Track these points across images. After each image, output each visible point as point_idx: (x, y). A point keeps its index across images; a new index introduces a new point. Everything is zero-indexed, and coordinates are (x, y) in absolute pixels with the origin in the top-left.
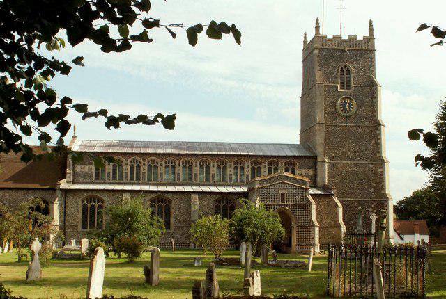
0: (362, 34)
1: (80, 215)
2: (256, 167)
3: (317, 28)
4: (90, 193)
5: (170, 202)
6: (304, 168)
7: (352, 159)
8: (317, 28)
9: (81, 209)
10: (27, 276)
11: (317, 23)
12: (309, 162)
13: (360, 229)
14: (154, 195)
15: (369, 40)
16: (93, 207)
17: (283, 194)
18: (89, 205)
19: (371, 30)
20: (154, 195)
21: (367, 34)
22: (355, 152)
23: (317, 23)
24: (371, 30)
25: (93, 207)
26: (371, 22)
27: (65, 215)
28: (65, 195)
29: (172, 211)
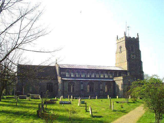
0: (136, 37)
3: (125, 34)
6: (124, 74)
8: (125, 34)
10: (84, 106)
11: (125, 33)
13: (6, 98)
15: (138, 38)
19: (138, 36)
20: (89, 82)
21: (137, 37)
23: (125, 33)
24: (138, 36)
26: (138, 34)
28: (63, 81)
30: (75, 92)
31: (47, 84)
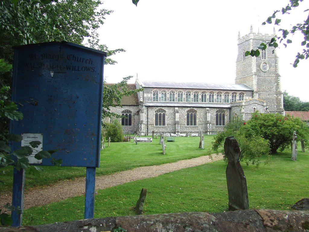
1: (154, 119)
2: (204, 94)
4: (159, 108)
5: (196, 111)
6: (248, 96)
7: (267, 92)
8: (251, 29)
9: (155, 115)
12: (250, 93)
14: (189, 109)
16: (160, 114)
17: (254, 108)
18: (159, 113)
22: (268, 89)
25: (126, 115)
27: (148, 118)
28: (147, 109)
29: (197, 116)
30: (166, 125)
31: (122, 112)
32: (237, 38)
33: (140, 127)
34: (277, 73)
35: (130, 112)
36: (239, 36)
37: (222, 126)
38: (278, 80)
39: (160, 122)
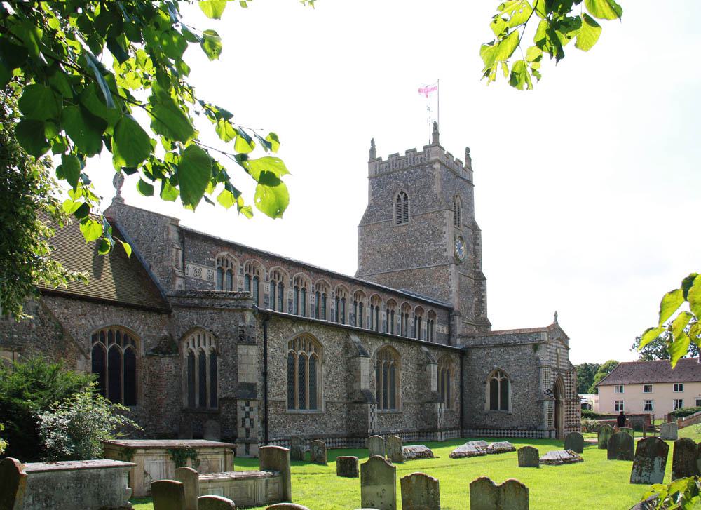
16: (114, 351)
32: (366, 157)
33: (241, 414)
34: (477, 270)
35: (128, 338)
36: (373, 151)
37: (297, 410)
38: (482, 288)
39: (302, 399)
